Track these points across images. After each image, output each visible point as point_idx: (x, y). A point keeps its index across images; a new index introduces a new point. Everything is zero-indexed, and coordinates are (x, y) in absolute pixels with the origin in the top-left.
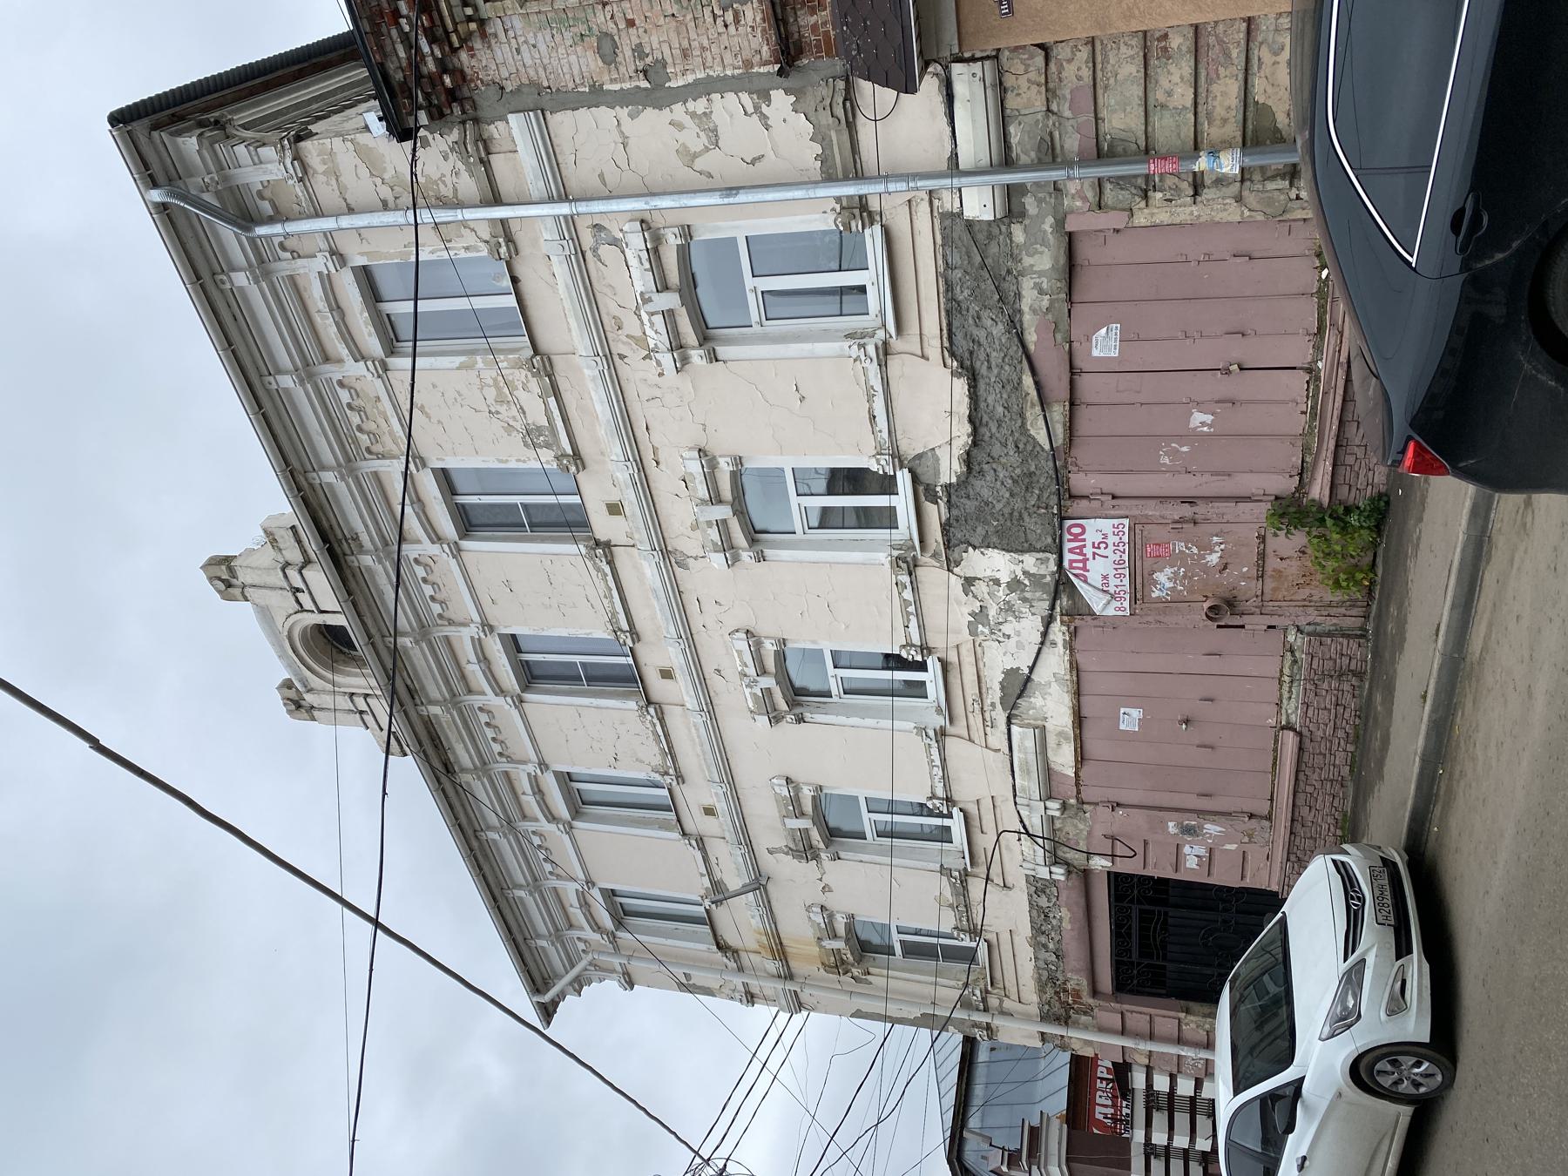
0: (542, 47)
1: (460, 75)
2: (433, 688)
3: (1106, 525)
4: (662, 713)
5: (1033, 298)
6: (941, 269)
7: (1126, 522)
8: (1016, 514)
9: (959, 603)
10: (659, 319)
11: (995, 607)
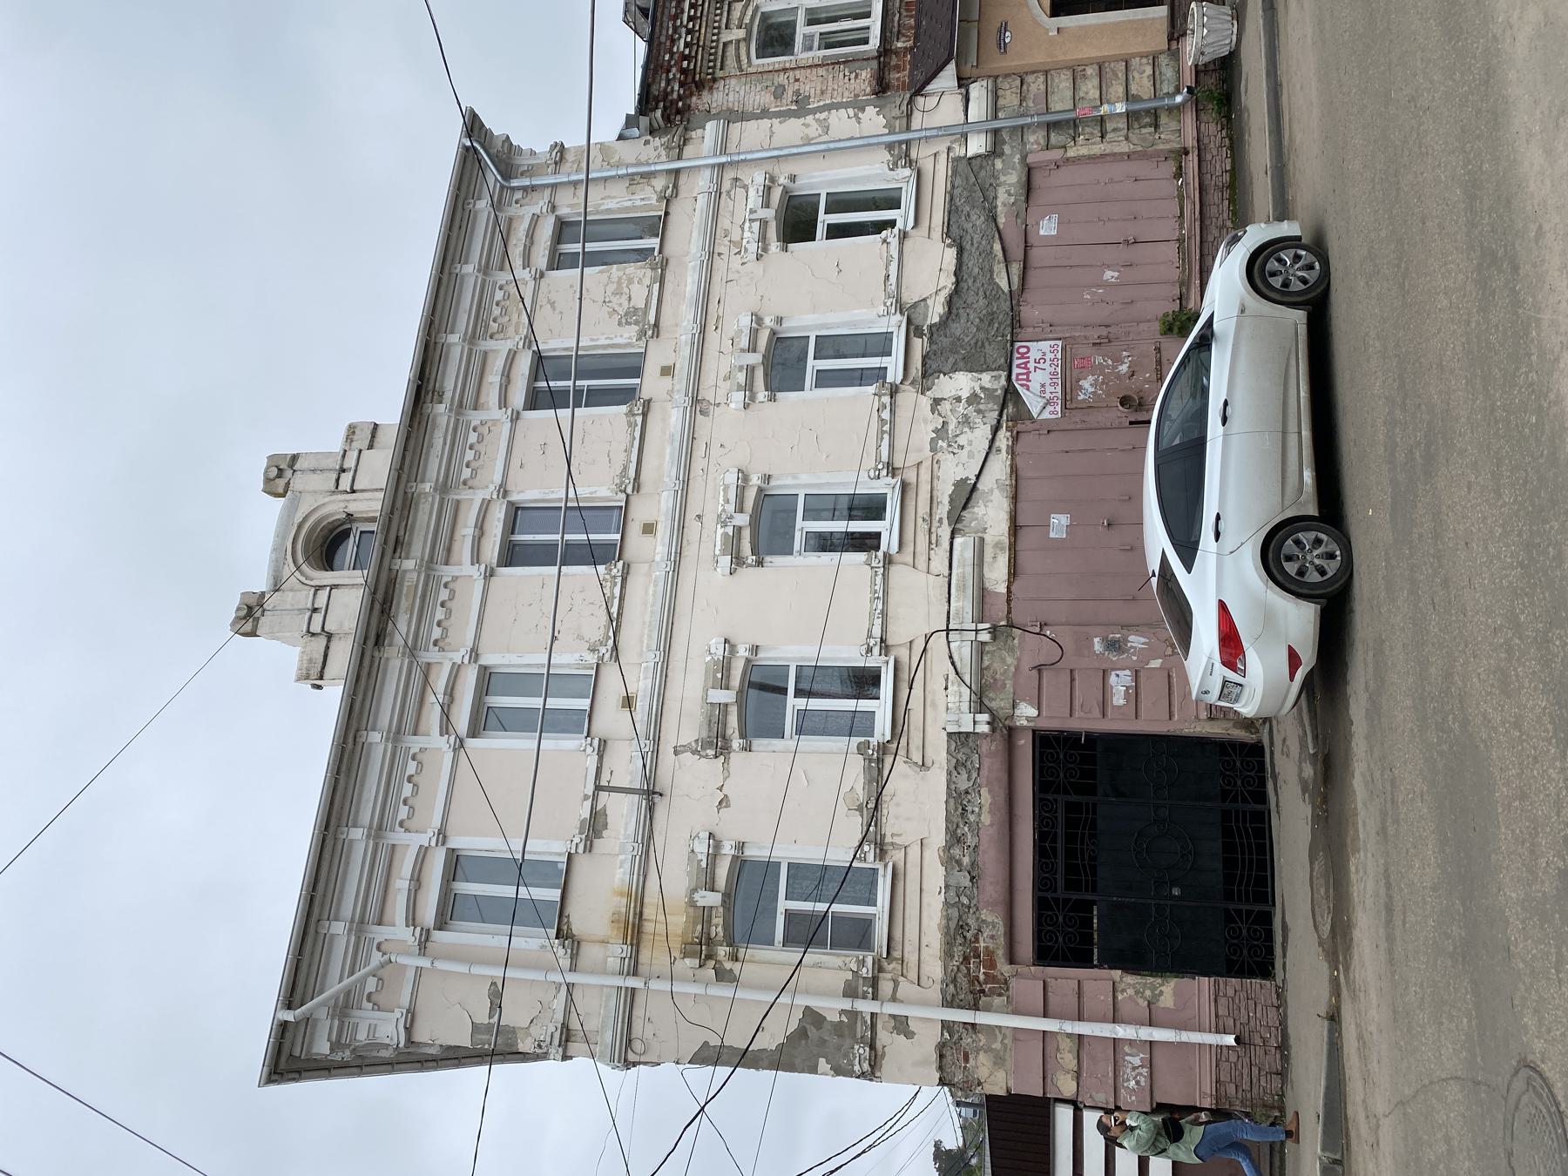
0: (742, 93)
1: (688, 108)
2: (419, 546)
3: (1045, 345)
4: (628, 573)
5: (1004, 198)
6: (949, 189)
7: (1060, 343)
8: (980, 343)
9: (925, 421)
10: (756, 225)
11: (955, 421)
